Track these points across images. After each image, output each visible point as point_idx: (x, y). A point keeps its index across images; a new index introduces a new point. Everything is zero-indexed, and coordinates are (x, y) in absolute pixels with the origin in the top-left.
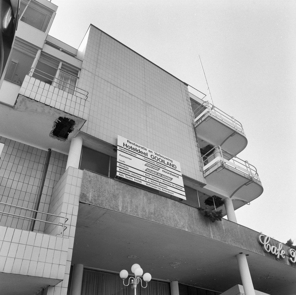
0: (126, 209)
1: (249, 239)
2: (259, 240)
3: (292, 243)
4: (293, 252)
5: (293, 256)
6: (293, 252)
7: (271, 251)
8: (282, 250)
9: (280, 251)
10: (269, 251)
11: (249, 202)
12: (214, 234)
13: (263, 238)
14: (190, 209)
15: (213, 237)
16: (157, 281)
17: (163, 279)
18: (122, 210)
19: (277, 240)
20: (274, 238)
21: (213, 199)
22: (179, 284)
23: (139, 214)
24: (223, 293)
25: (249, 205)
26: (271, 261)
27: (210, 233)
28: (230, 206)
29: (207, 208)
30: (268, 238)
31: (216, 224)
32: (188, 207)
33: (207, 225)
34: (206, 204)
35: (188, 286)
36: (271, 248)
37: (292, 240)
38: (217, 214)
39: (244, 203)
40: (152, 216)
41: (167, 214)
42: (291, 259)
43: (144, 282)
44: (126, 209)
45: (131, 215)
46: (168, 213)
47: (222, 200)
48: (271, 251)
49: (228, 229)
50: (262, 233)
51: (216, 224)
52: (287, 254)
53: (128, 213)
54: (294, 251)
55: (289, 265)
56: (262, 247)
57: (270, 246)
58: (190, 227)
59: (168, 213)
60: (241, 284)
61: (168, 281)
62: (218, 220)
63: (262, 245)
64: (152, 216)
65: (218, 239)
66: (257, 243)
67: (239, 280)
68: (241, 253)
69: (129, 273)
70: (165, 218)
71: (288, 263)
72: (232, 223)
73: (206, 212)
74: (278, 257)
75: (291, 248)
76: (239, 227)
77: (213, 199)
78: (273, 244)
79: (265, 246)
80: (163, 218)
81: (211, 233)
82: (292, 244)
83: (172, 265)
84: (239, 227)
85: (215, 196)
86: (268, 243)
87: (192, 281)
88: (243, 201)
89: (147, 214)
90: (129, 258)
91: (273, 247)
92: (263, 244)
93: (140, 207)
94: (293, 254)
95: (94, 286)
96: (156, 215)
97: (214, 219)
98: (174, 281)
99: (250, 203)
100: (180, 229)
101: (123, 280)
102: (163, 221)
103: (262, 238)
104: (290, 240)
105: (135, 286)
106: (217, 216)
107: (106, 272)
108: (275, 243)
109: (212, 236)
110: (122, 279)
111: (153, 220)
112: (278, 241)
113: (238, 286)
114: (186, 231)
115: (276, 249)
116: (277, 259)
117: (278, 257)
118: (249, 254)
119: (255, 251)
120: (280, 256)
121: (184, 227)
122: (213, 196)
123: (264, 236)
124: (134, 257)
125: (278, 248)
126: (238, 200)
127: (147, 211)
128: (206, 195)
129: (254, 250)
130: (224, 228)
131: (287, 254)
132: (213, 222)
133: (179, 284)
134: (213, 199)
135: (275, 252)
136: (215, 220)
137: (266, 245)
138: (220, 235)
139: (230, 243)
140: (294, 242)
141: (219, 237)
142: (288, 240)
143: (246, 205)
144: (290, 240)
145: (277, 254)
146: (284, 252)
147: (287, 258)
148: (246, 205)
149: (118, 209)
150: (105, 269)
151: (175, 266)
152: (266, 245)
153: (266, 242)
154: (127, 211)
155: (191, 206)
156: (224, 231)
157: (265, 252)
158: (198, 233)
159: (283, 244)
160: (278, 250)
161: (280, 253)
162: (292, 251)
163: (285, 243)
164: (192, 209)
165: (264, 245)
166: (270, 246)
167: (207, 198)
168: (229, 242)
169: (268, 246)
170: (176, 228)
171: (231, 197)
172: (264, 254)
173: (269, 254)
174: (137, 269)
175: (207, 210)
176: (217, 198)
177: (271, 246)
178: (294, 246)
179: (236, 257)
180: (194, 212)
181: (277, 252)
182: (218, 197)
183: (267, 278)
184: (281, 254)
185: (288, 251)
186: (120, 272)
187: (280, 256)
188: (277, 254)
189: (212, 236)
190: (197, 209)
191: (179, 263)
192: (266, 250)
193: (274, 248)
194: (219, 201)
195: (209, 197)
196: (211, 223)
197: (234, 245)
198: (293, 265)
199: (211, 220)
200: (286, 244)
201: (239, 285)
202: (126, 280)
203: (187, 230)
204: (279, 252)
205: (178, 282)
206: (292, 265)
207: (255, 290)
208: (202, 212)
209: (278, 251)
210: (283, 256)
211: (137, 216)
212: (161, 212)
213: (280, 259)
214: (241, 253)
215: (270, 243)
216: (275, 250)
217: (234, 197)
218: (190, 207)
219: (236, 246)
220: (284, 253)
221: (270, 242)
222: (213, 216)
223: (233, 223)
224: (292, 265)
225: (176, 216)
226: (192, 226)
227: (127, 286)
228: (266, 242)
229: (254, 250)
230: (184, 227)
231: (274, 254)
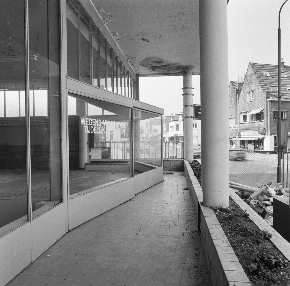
99: (107, 138)
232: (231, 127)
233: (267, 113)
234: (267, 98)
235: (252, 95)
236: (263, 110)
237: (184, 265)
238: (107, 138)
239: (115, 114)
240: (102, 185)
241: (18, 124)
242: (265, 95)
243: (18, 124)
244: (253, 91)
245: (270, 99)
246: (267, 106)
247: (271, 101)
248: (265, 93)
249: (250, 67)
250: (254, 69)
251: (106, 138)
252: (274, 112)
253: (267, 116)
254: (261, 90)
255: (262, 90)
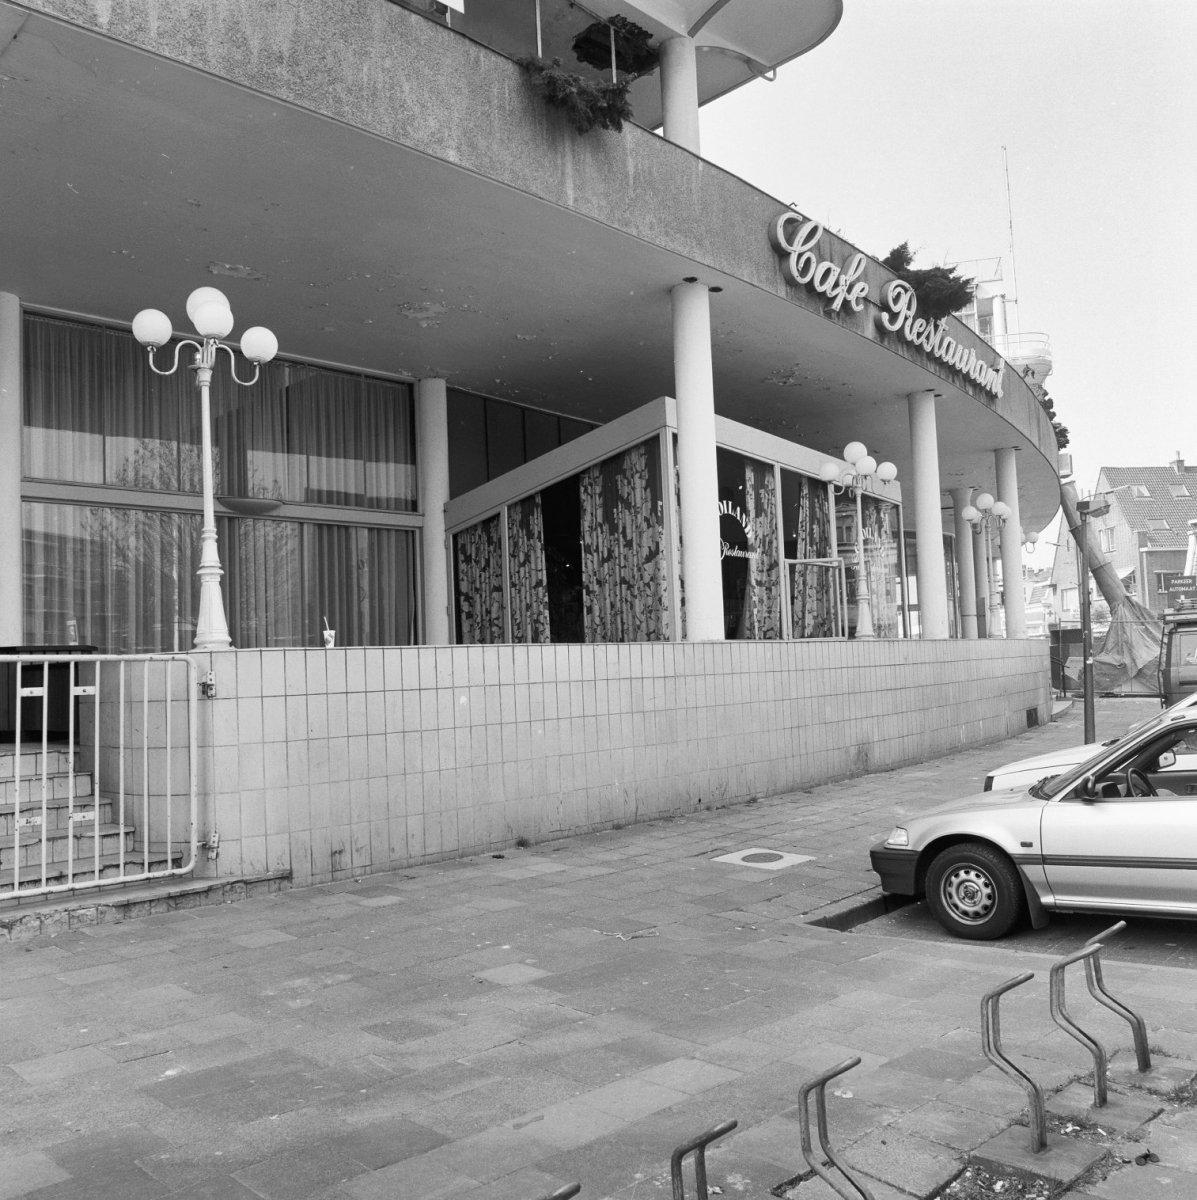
0: (138, 20)
1: (733, 225)
2: (778, 234)
3: (909, 261)
4: (899, 294)
5: (895, 309)
6: (903, 291)
7: (812, 279)
8: (858, 280)
9: (848, 283)
10: (807, 279)
11: (773, 68)
12: (578, 188)
13: (792, 226)
14: (482, 59)
15: (576, 200)
16: (359, 375)
17: (387, 370)
18: (111, 23)
19: (850, 242)
20: (841, 235)
21: (612, 32)
22: (449, 390)
23: (210, 52)
24: (605, 426)
25: (771, 80)
26: (805, 322)
27: (562, 183)
28: (684, 76)
29: (558, 65)
30: (814, 230)
31: (599, 146)
32: (473, 50)
33: (553, 143)
34: (580, 59)
35: (485, 399)
36: (817, 271)
37: (911, 249)
38: (604, 97)
39: (753, 69)
40: (282, 71)
41: (360, 70)
42: (885, 316)
43: (245, 365)
44: (138, 20)
45: (168, 55)
46: (365, 69)
47: (651, 42)
48: (812, 279)
49: (650, 173)
50: (795, 208)
51: (599, 146)
52: (875, 298)
53: (150, 40)
54: (906, 291)
55: (870, 337)
56: (780, 261)
57: (814, 259)
58: (472, 146)
59: (365, 69)
60: (673, 396)
61: (406, 376)
62: (605, 127)
63: (782, 255)
64: (282, 71)
65: (595, 208)
66: (765, 246)
67: (664, 383)
68: (692, 280)
69: (279, 350)
70: (349, 91)
71: (870, 331)
72: (674, 147)
73: (551, 82)
74: (837, 305)
75: (900, 277)
76: (701, 168)
77: (609, 35)
78: (831, 254)
79: (793, 258)
80: (339, 87)
81: (571, 183)
82: (908, 263)
83: (411, 314)
84: (701, 168)
85: (619, 21)
86: (809, 250)
87: (502, 383)
88: (748, 61)
89: (254, 60)
90: (215, 272)
91: (826, 265)
92: (789, 248)
93: (215, 19)
94: (896, 299)
95: (318, 417)
96: (302, 70)
97: (589, 120)
98: (430, 377)
99: (775, 74)
100: (421, 148)
101: (149, 349)
102: (338, 100)
103: (790, 229)
104: (904, 247)
105: (205, 377)
106: (601, 109)
107: (80, 323)
108: (838, 249)
109: (570, 193)
110: (141, 349)
111: (283, 93)
112: (852, 246)
113: (664, 403)
114: (451, 159)
115: (837, 274)
116: (829, 314)
117: (837, 305)
118: (722, 287)
119: (752, 275)
120: (846, 303)
121: (440, 141)
122: (612, 20)
123: (800, 218)
124: (236, 269)
125: (844, 270)
126: (722, 51)
127: (255, 44)
128: (581, 8)
129: (746, 273)
130: (631, 170)
131: (875, 298)
132: (581, 131)
133: (451, 392)
134: (612, 32)
135: (827, 287)
136: (591, 122)
137: (800, 255)
138: (607, 195)
139: (646, 233)
140: (915, 258)
141: (603, 203)
142: (896, 248)
143: (758, 83)
144: (904, 247)
145: (836, 296)
146: (867, 289)
147: (873, 311)
148: (760, 79)
149: (90, 13)
150: (321, 358)
151: (423, 319)
152: (800, 255)
153: (803, 245)
154: (140, 29)
155: (486, 47)
156: (631, 182)
157: (790, 282)
158: (506, 177)
159: (873, 259)
160: (843, 278)
161: (849, 291)
162: (899, 289)
163: (882, 258)
164: (488, 61)
165: (788, 254)
166: (814, 259)
167: (583, 25)
168: (645, 226)
169: (808, 261)
170: (402, 141)
171: (693, 32)
172: (782, 290)
173: (804, 292)
174: (211, 311)
175: (557, 73)
176: (631, 32)
177: (821, 259)
178: (914, 272)
179: (670, 294)
180: (500, 77)
181: (836, 285)
182: (634, 25)
183: (785, 383)
184: (852, 298)
185: (882, 287)
186: (132, 321)
187: (846, 303)
188: (836, 296)
189: (570, 193)
190: (516, 67)
191: (437, 308)
192: (795, 273)
193: (828, 272)
194: (641, 51)
195: (593, 22)
196: (573, 141)
197: (662, 241)
198: (886, 339)
199: (572, 121)
200: (887, 261)
201: (667, 398)
202: (164, 352)
203: (452, 156)
204: (846, 289)
205: (447, 382)
206: (882, 341)
207: (718, 416)
208: (537, 80)
209: (842, 282)
210: (857, 305)
211: (200, 65)
212: (330, 58)
213: (842, 314)
214: (692, 280)
215: (817, 248)
216: (831, 280)
217: (708, 37)
218: (483, 53)
219: (671, 246)
220: (863, 294)
221: (818, 245)
222: (581, 105)
223: (679, 150)
224: (882, 341)
225: (406, 87)
226: (482, 143)
227: (167, 373)
228: (803, 245)
229: (746, 273)
230: (440, 141)
231: (824, 293)
232: (1068, 610)
233: (1143, 579)
234: (1140, 546)
235: (1112, 537)
236: (1133, 572)
237: (449, 767)
238: (775, 74)
239: (514, 903)
240: (1015, 478)
241: (616, 857)
242: (1135, 540)
243: (616, 857)
244: (1112, 529)
245: (1145, 549)
246: (1141, 563)
247: (1148, 553)
248: (1136, 536)
249: (1103, 477)
250: (1113, 482)
251: (770, 74)
252: (1159, 575)
253: (1143, 584)
254: (1127, 528)
255: (1129, 529)
